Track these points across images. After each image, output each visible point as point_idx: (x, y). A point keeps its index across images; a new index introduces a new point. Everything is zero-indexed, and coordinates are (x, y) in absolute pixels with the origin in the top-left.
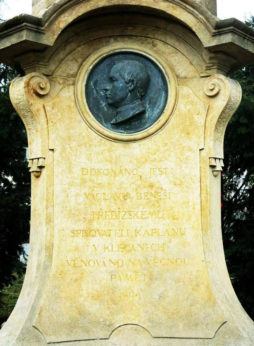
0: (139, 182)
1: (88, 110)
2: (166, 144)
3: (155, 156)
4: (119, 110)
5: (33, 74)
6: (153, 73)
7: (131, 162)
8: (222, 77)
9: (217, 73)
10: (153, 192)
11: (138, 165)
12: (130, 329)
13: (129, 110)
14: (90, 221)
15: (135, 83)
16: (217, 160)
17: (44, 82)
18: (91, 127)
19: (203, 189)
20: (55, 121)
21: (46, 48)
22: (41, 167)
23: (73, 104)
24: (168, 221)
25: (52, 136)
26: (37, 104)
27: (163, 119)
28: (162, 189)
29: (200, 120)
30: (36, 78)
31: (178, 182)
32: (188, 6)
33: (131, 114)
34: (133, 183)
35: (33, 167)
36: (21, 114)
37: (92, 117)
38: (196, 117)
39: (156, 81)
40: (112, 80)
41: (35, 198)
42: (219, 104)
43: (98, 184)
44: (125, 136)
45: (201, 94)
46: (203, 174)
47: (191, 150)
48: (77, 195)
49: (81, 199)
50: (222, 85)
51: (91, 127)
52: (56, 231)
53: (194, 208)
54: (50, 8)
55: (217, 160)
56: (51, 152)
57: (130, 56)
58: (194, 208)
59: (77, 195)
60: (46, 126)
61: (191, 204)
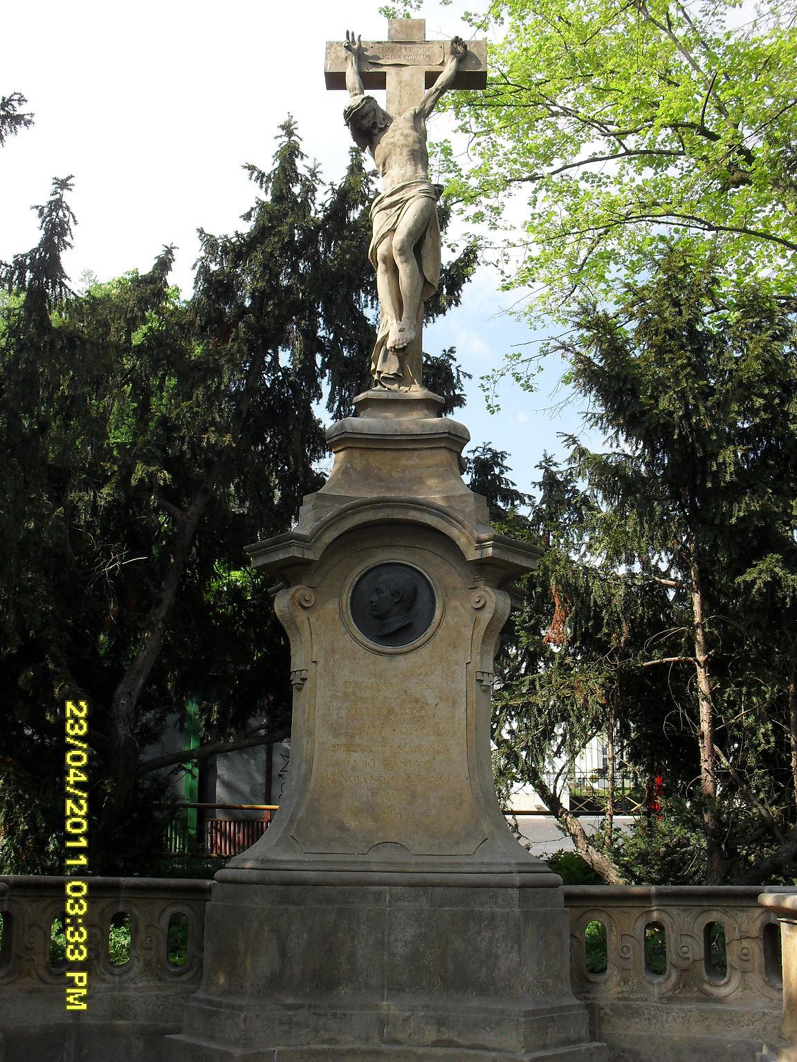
0: (404, 697)
1: (353, 622)
2: (433, 657)
3: (421, 670)
4: (386, 621)
5: (299, 587)
6: (728, 391)
7: (396, 675)
8: (488, 589)
9: (485, 585)
10: (418, 707)
11: (335, 716)
12: (608, 784)
13: (395, 623)
14: (352, 736)
15: (401, 594)
16: (486, 675)
17: (309, 594)
18: (355, 639)
19: (469, 703)
20: (318, 633)
21: (307, 563)
22: (304, 679)
23: (337, 616)
24: (433, 737)
25: (316, 648)
26: (302, 616)
27: (430, 631)
28: (427, 704)
29: (467, 633)
30: (299, 590)
31: (444, 697)
32: (451, 520)
33: (398, 625)
34: (397, 698)
35: (295, 679)
36: (285, 625)
37: (357, 629)
38: (463, 630)
39: (423, 596)
40: (378, 591)
41: (296, 711)
42: (486, 616)
43: (361, 698)
44: (390, 649)
45: (468, 606)
46: (469, 689)
47: (457, 664)
48: (339, 708)
49: (343, 713)
50: (487, 597)
51: (355, 639)
52: (317, 744)
53: (459, 724)
54: (429, 424)
55: (486, 675)
56: (314, 664)
57: (400, 567)
58: (459, 724)
59: (339, 708)
60: (309, 638)
61: (456, 719)
